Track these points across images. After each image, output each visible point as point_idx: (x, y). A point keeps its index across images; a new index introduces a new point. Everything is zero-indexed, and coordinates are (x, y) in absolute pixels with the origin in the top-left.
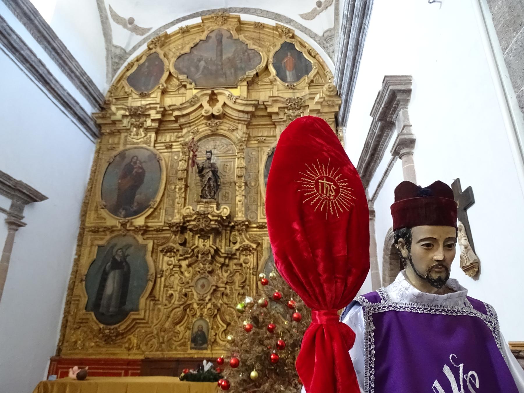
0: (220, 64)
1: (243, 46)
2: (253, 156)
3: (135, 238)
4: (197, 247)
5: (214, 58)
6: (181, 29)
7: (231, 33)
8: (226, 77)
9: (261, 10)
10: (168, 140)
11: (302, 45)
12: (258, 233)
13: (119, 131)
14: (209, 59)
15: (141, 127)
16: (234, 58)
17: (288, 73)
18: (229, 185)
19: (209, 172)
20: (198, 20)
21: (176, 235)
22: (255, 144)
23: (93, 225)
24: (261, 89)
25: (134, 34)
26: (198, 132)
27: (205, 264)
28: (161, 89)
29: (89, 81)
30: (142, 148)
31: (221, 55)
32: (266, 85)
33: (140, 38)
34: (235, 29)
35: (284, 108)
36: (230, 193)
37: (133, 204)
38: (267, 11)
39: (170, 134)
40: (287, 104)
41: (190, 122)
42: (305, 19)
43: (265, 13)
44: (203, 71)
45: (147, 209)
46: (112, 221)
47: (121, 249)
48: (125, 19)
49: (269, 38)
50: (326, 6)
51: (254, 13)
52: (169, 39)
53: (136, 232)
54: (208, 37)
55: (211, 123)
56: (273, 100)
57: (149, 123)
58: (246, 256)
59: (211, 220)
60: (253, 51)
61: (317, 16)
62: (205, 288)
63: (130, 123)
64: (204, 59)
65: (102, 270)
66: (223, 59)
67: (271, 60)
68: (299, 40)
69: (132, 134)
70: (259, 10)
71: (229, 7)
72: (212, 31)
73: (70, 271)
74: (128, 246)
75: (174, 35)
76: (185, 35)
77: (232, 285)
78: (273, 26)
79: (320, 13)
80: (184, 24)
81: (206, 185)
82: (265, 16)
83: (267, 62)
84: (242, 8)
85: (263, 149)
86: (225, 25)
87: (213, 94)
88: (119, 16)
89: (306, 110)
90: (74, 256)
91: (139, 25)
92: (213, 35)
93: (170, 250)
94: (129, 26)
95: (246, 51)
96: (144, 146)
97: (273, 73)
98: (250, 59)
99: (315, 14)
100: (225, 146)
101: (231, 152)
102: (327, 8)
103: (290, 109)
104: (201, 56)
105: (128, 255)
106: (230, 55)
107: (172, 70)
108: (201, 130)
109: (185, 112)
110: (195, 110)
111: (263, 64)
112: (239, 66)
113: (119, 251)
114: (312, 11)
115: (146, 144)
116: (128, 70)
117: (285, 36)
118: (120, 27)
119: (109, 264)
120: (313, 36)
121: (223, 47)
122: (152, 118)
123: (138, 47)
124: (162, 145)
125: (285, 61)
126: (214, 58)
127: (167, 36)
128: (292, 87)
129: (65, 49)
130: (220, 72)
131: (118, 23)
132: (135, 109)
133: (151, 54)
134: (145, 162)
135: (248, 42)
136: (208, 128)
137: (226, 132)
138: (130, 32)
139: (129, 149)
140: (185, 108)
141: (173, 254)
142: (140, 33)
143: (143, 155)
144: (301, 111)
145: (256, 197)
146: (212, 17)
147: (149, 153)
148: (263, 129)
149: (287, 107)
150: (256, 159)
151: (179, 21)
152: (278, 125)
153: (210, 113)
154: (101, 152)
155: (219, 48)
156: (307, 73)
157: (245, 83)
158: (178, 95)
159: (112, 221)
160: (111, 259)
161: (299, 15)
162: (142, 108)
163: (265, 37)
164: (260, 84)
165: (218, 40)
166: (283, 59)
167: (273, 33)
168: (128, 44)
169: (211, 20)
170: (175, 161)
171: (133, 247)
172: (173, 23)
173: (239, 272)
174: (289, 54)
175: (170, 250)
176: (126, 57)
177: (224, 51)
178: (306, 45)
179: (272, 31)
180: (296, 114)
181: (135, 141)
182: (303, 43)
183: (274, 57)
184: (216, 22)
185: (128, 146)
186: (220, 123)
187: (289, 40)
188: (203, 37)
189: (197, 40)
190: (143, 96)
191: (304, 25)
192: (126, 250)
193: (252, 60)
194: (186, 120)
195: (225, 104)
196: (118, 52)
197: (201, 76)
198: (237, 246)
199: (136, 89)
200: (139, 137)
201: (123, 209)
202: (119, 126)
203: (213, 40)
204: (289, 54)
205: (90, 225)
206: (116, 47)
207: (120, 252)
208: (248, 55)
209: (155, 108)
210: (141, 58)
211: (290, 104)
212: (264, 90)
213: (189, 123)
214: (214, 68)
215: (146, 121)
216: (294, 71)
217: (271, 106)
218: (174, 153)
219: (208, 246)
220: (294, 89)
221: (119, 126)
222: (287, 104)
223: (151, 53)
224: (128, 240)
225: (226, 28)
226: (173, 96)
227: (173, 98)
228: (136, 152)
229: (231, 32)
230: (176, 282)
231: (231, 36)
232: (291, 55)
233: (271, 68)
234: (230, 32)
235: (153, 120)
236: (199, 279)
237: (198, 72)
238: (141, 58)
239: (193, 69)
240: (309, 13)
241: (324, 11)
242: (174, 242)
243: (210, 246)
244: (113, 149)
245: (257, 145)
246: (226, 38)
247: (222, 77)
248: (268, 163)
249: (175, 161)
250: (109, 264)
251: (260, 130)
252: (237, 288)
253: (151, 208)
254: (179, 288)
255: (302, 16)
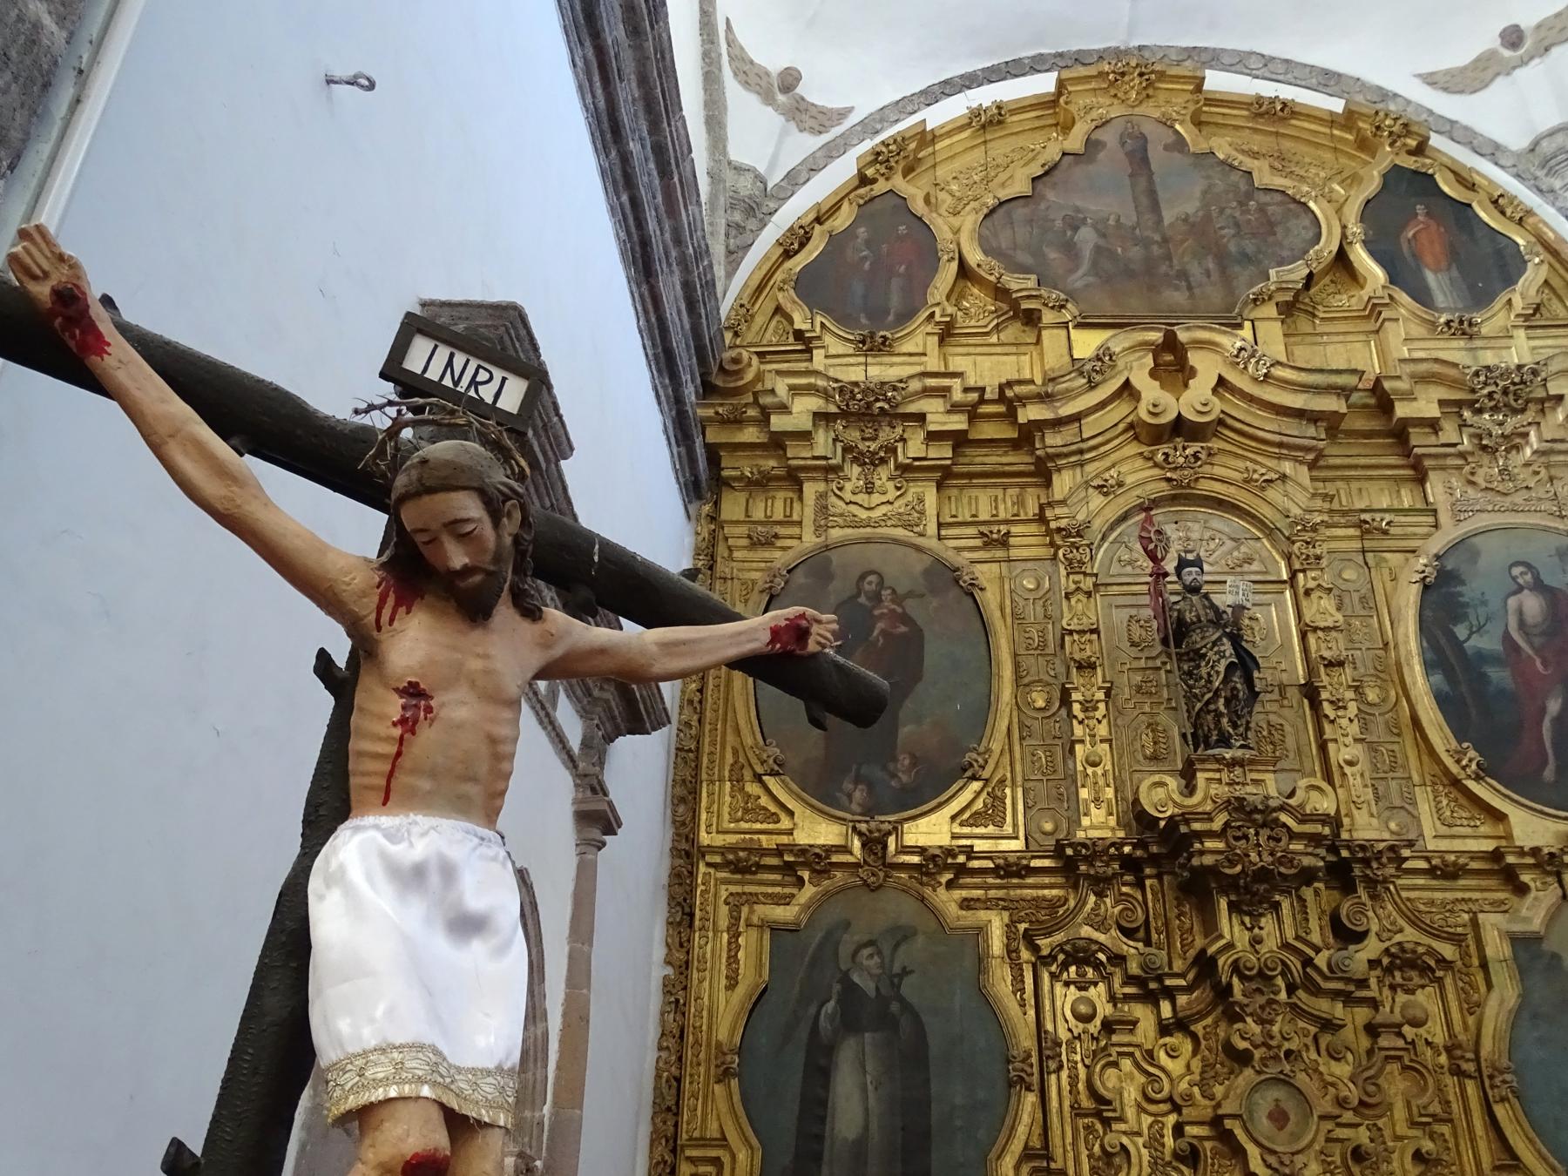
0: (1157, 237)
1: (1235, 177)
2: (1350, 587)
3: (923, 899)
4: (1230, 946)
5: (1130, 218)
6: (976, 113)
7: (1177, 132)
8: (1190, 288)
9: (1263, 56)
10: (983, 516)
11: (1466, 181)
12: (1438, 895)
13: (793, 479)
14: (1111, 222)
15: (883, 461)
16: (1208, 218)
17: (1430, 278)
18: (1275, 696)
19: (1220, 639)
20: (1044, 83)
21: (1100, 895)
22: (1350, 538)
23: (732, 839)
24: (1328, 334)
25: (792, 126)
26: (1120, 484)
27: (1272, 1022)
28: (938, 323)
29: (707, 282)
30: (896, 541)
31: (1155, 207)
32: (1346, 318)
33: (813, 143)
34: (1188, 118)
35: (1459, 404)
36: (1287, 728)
37: (894, 759)
38: (1287, 61)
39: (991, 492)
40: (1473, 391)
41: (1084, 446)
42: (1445, 89)
43: (1281, 68)
44: (1095, 264)
45: (960, 783)
46: (818, 832)
47: (871, 943)
48: (768, 74)
49: (1319, 152)
50: (1546, 43)
51: (1238, 67)
52: (930, 150)
53: (928, 874)
54: (1092, 145)
55: (1171, 452)
56: (1413, 376)
57: (915, 446)
58: (1411, 992)
59: (1293, 836)
60: (1278, 197)
61: (1500, 81)
62: (1290, 1126)
63: (839, 446)
64: (1089, 221)
65: (803, 1033)
66: (1167, 221)
67: (1355, 229)
68: (1445, 160)
69: (849, 486)
70: (1254, 58)
71: (1135, 43)
72: (1106, 123)
73: (652, 1033)
74: (902, 935)
75: (949, 134)
76: (989, 137)
77: (1381, 1117)
78: (1331, 113)
79: (1514, 68)
80: (985, 96)
81: (1217, 693)
82: (1281, 77)
83: (1344, 236)
84: (1186, 49)
85: (1386, 560)
86: (1151, 102)
87: (1170, 344)
88: (752, 62)
89: (1549, 416)
90: (659, 971)
91: (810, 99)
92: (1109, 136)
93: (1080, 955)
94: (781, 98)
95: (1249, 195)
96: (900, 532)
97: (1375, 276)
98: (1271, 226)
99: (1490, 72)
100: (1229, 544)
101: (1255, 567)
102: (1547, 50)
103: (1480, 411)
104: (1078, 210)
105: (905, 972)
106: (1191, 207)
107: (974, 256)
108: (1129, 480)
109: (1067, 410)
110: (1102, 405)
111: (1328, 246)
112: (1232, 248)
113: (866, 952)
114: (1478, 60)
115: (908, 526)
116: (788, 254)
117: (1391, 145)
118: (753, 100)
119: (831, 1005)
120: (1489, 151)
121: (1157, 179)
122: (932, 428)
123: (804, 176)
124: (972, 531)
125: (1410, 234)
126: (1130, 218)
127: (926, 138)
128: (1464, 330)
129: (686, 151)
130: (1163, 268)
131: (746, 84)
132: (867, 391)
133: (872, 199)
134: (910, 594)
135: (1249, 163)
136: (1156, 471)
137: (1232, 490)
138: (782, 118)
139: (843, 544)
140: (1069, 395)
141: (1090, 972)
142: (811, 123)
143: (902, 570)
144: (1530, 416)
145: (1395, 747)
146: (1102, 75)
147: (927, 561)
148: (1365, 484)
149: (1470, 404)
150: (1363, 599)
151: (970, 81)
152: (1434, 469)
153: (1169, 417)
154: (721, 550)
155: (1142, 183)
156: (1509, 280)
157: (1270, 310)
158: (999, 350)
159: (818, 832)
160: (837, 987)
161: (1419, 76)
162: (895, 389)
163: (1302, 148)
164: (1322, 315)
165: (1130, 155)
166: (1403, 227)
167: (1332, 135)
168: (773, 164)
169: (1093, 85)
170: (1031, 596)
171: (920, 940)
172: (949, 88)
173: (1399, 1058)
174: (1420, 208)
175: (1080, 955)
176: (765, 210)
177: (1162, 195)
178: (1477, 179)
179: (1327, 131)
180: (1508, 429)
181: (863, 514)
182: (1465, 174)
183: (1362, 219)
184: (1113, 92)
185: (836, 534)
186: (1210, 455)
187: (1410, 163)
188: (1075, 142)
189: (1052, 153)
190: (874, 346)
191: (1438, 110)
192: (897, 946)
193: (1279, 230)
194: (1070, 439)
195: (1221, 382)
196: (745, 186)
197: (1091, 279)
198: (1372, 948)
199: (844, 320)
200: (876, 498)
201: (857, 780)
202: (798, 454)
203: (1112, 159)
204: (1420, 208)
205: (720, 840)
206: (739, 169)
207: (871, 956)
208: (1262, 209)
209: (944, 392)
210: (835, 208)
211: (1485, 392)
212: (1341, 338)
213: (1081, 452)
214: (1136, 252)
215: (903, 440)
216: (1455, 273)
217: (1409, 396)
218: (1021, 566)
219: (1271, 944)
220: (1471, 337)
221: (798, 454)
222: (1473, 391)
223: (874, 193)
224: (895, 907)
225: (1157, 114)
226: (979, 350)
227: (979, 358)
228: (874, 557)
229: (1178, 127)
230: (1131, 1094)
231: (1180, 144)
232: (1428, 214)
233: (1361, 257)
234: (1172, 127)
235: (933, 437)
236: (1255, 1088)
237: (1077, 268)
238: (835, 208)
239: (1053, 255)
240: (1463, 70)
241: (1537, 61)
242: (1101, 926)
243: (1286, 946)
244: (769, 542)
245: (1357, 545)
246: (1161, 148)
247: (1177, 288)
248: (1428, 613)
249: (1031, 596)
250: (831, 1005)
251: (1355, 485)
252: (1402, 1128)
253: (974, 778)
254: (1147, 1120)
255: (1430, 80)
